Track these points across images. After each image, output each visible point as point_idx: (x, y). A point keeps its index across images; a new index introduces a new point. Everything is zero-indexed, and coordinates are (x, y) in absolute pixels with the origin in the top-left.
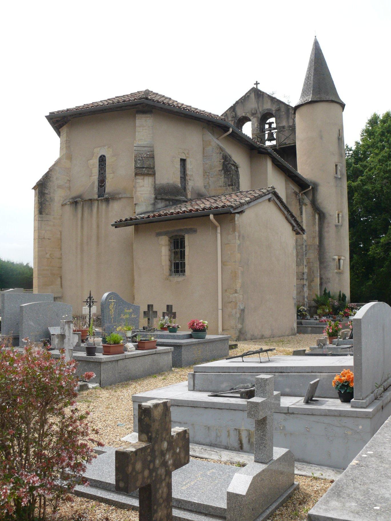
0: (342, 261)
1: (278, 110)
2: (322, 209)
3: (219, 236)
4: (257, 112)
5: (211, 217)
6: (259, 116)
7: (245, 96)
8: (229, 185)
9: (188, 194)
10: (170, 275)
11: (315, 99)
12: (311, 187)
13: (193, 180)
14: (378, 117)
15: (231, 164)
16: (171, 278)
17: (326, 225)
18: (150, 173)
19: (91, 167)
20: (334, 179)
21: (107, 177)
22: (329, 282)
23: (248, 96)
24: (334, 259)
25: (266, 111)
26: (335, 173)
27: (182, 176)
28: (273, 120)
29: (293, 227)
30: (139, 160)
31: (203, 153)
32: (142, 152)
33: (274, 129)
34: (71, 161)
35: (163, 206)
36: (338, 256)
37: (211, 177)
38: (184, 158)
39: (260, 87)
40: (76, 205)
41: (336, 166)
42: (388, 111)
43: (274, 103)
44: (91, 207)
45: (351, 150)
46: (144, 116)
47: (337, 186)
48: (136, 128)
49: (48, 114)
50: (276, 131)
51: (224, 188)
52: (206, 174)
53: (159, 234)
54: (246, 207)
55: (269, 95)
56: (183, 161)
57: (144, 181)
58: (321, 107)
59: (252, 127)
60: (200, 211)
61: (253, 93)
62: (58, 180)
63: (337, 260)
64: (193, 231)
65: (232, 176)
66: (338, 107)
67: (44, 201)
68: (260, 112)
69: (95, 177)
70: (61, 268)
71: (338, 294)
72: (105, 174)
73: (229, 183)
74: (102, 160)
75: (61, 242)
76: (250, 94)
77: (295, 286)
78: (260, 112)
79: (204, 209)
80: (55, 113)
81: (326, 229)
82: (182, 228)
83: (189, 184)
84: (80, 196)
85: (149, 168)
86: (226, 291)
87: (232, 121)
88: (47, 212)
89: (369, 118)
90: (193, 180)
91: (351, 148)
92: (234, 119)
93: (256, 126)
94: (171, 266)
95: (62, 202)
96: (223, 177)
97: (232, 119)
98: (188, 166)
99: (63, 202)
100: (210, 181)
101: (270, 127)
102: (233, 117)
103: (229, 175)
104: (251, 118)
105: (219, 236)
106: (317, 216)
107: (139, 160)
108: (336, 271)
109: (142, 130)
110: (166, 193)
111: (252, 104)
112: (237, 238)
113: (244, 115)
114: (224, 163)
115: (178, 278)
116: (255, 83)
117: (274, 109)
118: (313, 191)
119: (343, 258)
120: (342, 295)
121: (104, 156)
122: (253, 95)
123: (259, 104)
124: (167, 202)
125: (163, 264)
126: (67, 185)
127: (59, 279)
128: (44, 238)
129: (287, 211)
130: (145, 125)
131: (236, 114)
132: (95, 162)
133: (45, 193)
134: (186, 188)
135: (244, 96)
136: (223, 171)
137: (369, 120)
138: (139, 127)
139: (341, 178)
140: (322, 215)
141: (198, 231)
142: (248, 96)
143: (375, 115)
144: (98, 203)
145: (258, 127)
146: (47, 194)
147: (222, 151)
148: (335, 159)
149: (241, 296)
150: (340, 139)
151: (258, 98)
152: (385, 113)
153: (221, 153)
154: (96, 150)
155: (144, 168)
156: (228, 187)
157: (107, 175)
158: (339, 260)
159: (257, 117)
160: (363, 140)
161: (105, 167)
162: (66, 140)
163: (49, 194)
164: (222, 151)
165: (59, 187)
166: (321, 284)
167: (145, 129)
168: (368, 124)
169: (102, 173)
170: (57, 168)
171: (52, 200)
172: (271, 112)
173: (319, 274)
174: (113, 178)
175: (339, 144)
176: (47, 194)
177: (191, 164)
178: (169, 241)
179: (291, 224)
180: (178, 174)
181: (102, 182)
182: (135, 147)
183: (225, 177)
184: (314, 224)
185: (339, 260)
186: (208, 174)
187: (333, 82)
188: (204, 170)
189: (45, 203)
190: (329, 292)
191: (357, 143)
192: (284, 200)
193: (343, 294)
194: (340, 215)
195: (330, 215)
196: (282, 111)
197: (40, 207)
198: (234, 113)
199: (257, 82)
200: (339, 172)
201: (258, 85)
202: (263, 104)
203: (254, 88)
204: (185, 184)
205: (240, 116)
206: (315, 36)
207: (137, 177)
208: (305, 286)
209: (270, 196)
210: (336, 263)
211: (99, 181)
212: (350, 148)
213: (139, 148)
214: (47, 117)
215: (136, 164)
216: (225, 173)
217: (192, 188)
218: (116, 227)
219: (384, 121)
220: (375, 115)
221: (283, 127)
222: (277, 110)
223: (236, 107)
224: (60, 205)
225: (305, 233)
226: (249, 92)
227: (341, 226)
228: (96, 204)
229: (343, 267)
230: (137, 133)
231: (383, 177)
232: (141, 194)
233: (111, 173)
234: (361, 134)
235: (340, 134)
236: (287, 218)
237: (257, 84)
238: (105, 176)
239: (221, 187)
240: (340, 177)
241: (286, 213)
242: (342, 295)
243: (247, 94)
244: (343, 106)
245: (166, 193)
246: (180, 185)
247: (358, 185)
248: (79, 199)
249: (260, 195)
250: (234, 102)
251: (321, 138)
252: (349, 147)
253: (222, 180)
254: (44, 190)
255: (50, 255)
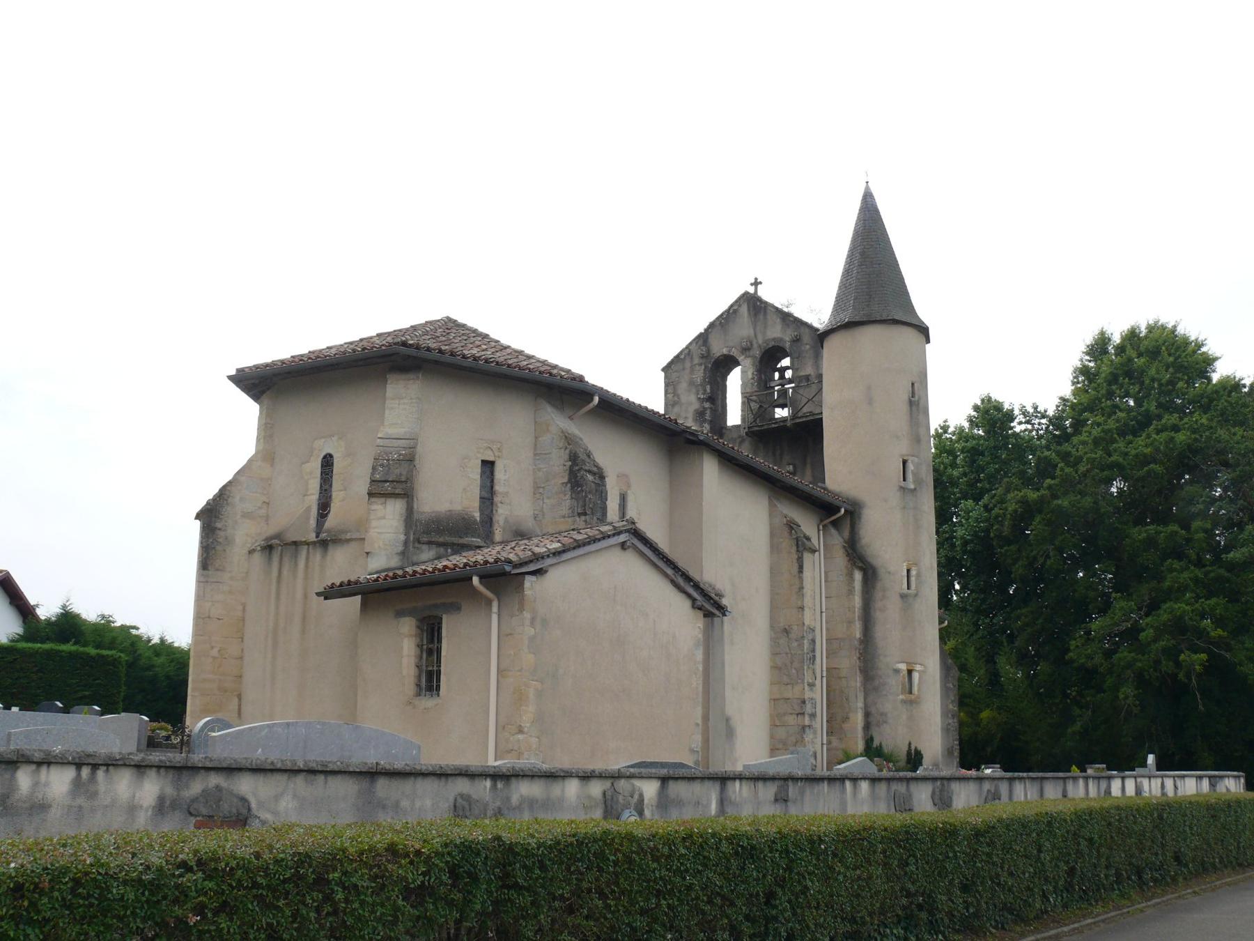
0: (916, 676)
1: (797, 340)
2: (870, 560)
3: (495, 618)
4: (752, 345)
5: (475, 580)
6: (757, 353)
7: (728, 311)
8: (579, 515)
9: (497, 532)
10: (418, 694)
11: (857, 319)
12: (843, 511)
13: (510, 504)
14: (1110, 340)
15: (586, 471)
16: (417, 701)
17: (878, 594)
18: (397, 492)
19: (306, 477)
20: (898, 493)
21: (333, 497)
22: (886, 722)
23: (735, 312)
24: (897, 671)
25: (772, 344)
26: (902, 479)
27: (486, 495)
28: (786, 362)
29: (694, 600)
30: (382, 465)
31: (535, 448)
32: (392, 449)
33: (790, 381)
34: (272, 465)
35: (431, 558)
36: (907, 663)
37: (548, 498)
38: (491, 459)
39: (765, 294)
40: (270, 553)
41: (905, 462)
42: (1133, 324)
43: (788, 325)
44: (296, 557)
45: (1043, 417)
46: (403, 376)
47: (904, 508)
48: (387, 402)
49: (233, 372)
50: (793, 385)
51: (570, 520)
52: (538, 490)
53: (400, 614)
54: (549, 561)
55: (777, 308)
56: (488, 466)
57: (385, 508)
58: (870, 337)
59: (742, 379)
60: (460, 568)
61: (746, 304)
62: (240, 504)
63: (905, 673)
64: (455, 608)
65: (586, 496)
66: (910, 334)
67: (212, 542)
68: (760, 346)
69: (313, 499)
70: (241, 677)
71: (905, 749)
72: (331, 491)
73: (580, 511)
74: (328, 462)
75: (244, 625)
76: (740, 306)
77: (697, 725)
78: (760, 346)
79: (466, 565)
80: (246, 370)
81: (878, 604)
82: (439, 601)
83: (500, 511)
84: (278, 536)
85: (397, 482)
86: (504, 728)
87: (701, 365)
88: (217, 565)
89: (1089, 340)
90: (510, 504)
91: (1046, 411)
92: (704, 361)
93: (750, 376)
94: (419, 677)
95: (249, 545)
96: (568, 496)
97: (701, 361)
98: (499, 474)
99: (253, 545)
100: (544, 506)
101: (782, 377)
102: (703, 357)
103: (579, 493)
104: (740, 359)
105: (495, 618)
106: (858, 576)
107: (382, 465)
108: (901, 697)
109: (396, 406)
110: (439, 531)
111: (743, 328)
112: (527, 622)
113: (725, 351)
114: (571, 467)
115: (428, 702)
116: (753, 281)
117: (787, 339)
118: (851, 520)
119: (918, 667)
120: (913, 751)
121: (331, 456)
122: (744, 309)
123: (758, 328)
124: (442, 550)
125: (405, 672)
126: (263, 512)
127: (236, 700)
128: (209, 617)
129: (673, 569)
130: (404, 395)
131: (709, 351)
132: (315, 466)
133: (216, 528)
134: (494, 520)
135: (726, 311)
136: (569, 485)
137: (1088, 346)
138: (393, 399)
139: (915, 489)
140: (871, 571)
141: (463, 607)
142: (735, 312)
143: (1102, 333)
144: (308, 549)
145: (753, 379)
146: (220, 529)
147: (569, 444)
148: (902, 447)
149: (534, 740)
150: (917, 403)
151: (756, 315)
152: (1126, 329)
153: (566, 448)
154: (318, 443)
155: (386, 481)
156: (578, 519)
157: (334, 494)
158: (910, 672)
159: (754, 357)
160: (1075, 393)
161: (332, 477)
162: (266, 424)
163: (225, 530)
164: (569, 444)
165: (246, 515)
166: (867, 727)
167: (404, 404)
168: (1087, 353)
169: (326, 490)
170: (242, 479)
171: (229, 541)
172: (781, 345)
173: (860, 704)
174: (343, 500)
175: (911, 414)
176: (220, 529)
177: (505, 471)
178: (418, 627)
179: (689, 596)
180: (475, 492)
181: (324, 507)
182: (379, 440)
183: (572, 498)
184: (851, 592)
185: (910, 672)
186: (541, 490)
187: (902, 279)
188: (535, 483)
189: (214, 548)
190: (881, 744)
191: (1063, 399)
192: (663, 545)
193: (916, 749)
194: (913, 573)
195: (889, 573)
196: (805, 342)
197: (205, 555)
198: (704, 349)
199: (756, 279)
200: (910, 476)
201: (759, 286)
202: (765, 327)
203: (746, 293)
204: (492, 511)
205: (718, 355)
206: (867, 182)
207: (373, 500)
208: (807, 729)
209: (622, 538)
210: (901, 679)
211: (319, 505)
212: (1043, 411)
213: (387, 442)
214: (231, 378)
215: (373, 474)
216: (572, 488)
217: (506, 521)
218: (326, 598)
219: (1120, 349)
220: (1102, 333)
221: (807, 378)
222: (794, 341)
223: (710, 336)
224: (245, 551)
225: (727, 613)
226: (736, 301)
227: (916, 595)
228: (303, 551)
229: (919, 690)
230: (387, 412)
231: (1097, 478)
232: (379, 533)
233: (341, 491)
234: (1072, 378)
235: (916, 392)
236: (674, 583)
237: (756, 283)
238: (331, 497)
239: (564, 517)
240: (912, 487)
241: (670, 571)
242: (913, 751)
243: (732, 306)
244: (924, 331)
245: (439, 531)
246: (477, 515)
247: (1042, 500)
248: (277, 541)
249: (589, 537)
250: (706, 325)
251: (870, 401)
252: (1041, 409)
253: (567, 503)
254: (215, 522)
255: (219, 651)
